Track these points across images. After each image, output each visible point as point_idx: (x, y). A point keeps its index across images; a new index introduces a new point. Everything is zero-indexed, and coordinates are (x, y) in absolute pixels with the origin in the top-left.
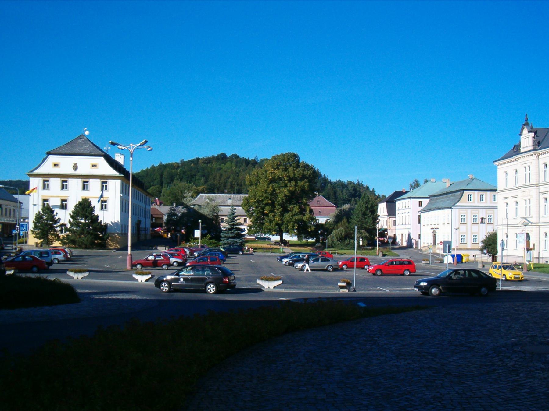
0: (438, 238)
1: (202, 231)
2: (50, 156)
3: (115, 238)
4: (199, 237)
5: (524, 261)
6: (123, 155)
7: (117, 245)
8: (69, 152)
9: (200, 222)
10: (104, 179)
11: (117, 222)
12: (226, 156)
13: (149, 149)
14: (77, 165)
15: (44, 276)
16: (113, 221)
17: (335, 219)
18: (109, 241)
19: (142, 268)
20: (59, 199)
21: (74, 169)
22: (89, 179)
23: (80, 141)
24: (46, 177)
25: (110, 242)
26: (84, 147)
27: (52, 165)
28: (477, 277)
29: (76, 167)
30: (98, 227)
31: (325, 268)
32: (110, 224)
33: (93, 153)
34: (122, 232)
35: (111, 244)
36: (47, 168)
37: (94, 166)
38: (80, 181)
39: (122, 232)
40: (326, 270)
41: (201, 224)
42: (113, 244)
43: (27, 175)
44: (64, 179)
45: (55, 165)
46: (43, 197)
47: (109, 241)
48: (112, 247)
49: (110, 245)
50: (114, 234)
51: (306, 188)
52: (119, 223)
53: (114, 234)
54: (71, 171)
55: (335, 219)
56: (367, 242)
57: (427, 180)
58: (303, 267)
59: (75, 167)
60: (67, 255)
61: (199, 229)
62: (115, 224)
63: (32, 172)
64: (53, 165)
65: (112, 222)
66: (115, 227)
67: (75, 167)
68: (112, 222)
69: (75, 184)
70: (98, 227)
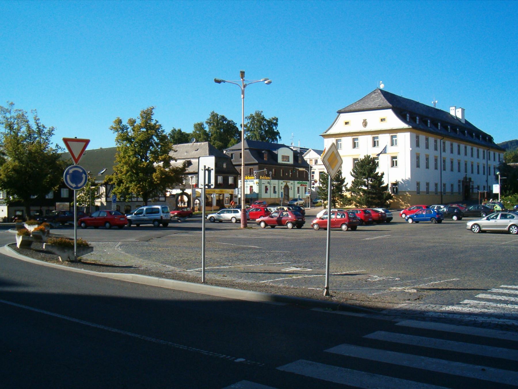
0: (206, 152)
1: (216, 174)
2: (341, 114)
3: (407, 197)
4: (498, 193)
5: (294, 195)
6: (460, 108)
7: (409, 205)
8: (362, 108)
9: (499, 174)
10: (393, 132)
11: (408, 179)
13: (266, 82)
14: (367, 121)
16: (404, 179)
18: (400, 200)
19: (293, 227)
21: (364, 125)
22: (378, 134)
23: (373, 95)
25: (401, 201)
26: (375, 101)
29: (366, 123)
30: (376, 185)
31: (506, 229)
32: (401, 182)
33: (381, 107)
34: (441, 191)
35: (402, 204)
36: (338, 128)
38: (370, 138)
39: (441, 191)
40: (508, 232)
41: (501, 177)
42: (405, 203)
43: (321, 136)
45: (346, 123)
47: (400, 200)
48: (403, 206)
49: (402, 205)
50: (405, 192)
52: (410, 180)
53: (405, 192)
54: (361, 128)
56: (353, 179)
58: (473, 227)
59: (365, 124)
61: (498, 184)
62: (406, 182)
64: (344, 123)
65: (402, 180)
66: (407, 185)
67: (365, 124)
68: (402, 180)
70: (376, 185)
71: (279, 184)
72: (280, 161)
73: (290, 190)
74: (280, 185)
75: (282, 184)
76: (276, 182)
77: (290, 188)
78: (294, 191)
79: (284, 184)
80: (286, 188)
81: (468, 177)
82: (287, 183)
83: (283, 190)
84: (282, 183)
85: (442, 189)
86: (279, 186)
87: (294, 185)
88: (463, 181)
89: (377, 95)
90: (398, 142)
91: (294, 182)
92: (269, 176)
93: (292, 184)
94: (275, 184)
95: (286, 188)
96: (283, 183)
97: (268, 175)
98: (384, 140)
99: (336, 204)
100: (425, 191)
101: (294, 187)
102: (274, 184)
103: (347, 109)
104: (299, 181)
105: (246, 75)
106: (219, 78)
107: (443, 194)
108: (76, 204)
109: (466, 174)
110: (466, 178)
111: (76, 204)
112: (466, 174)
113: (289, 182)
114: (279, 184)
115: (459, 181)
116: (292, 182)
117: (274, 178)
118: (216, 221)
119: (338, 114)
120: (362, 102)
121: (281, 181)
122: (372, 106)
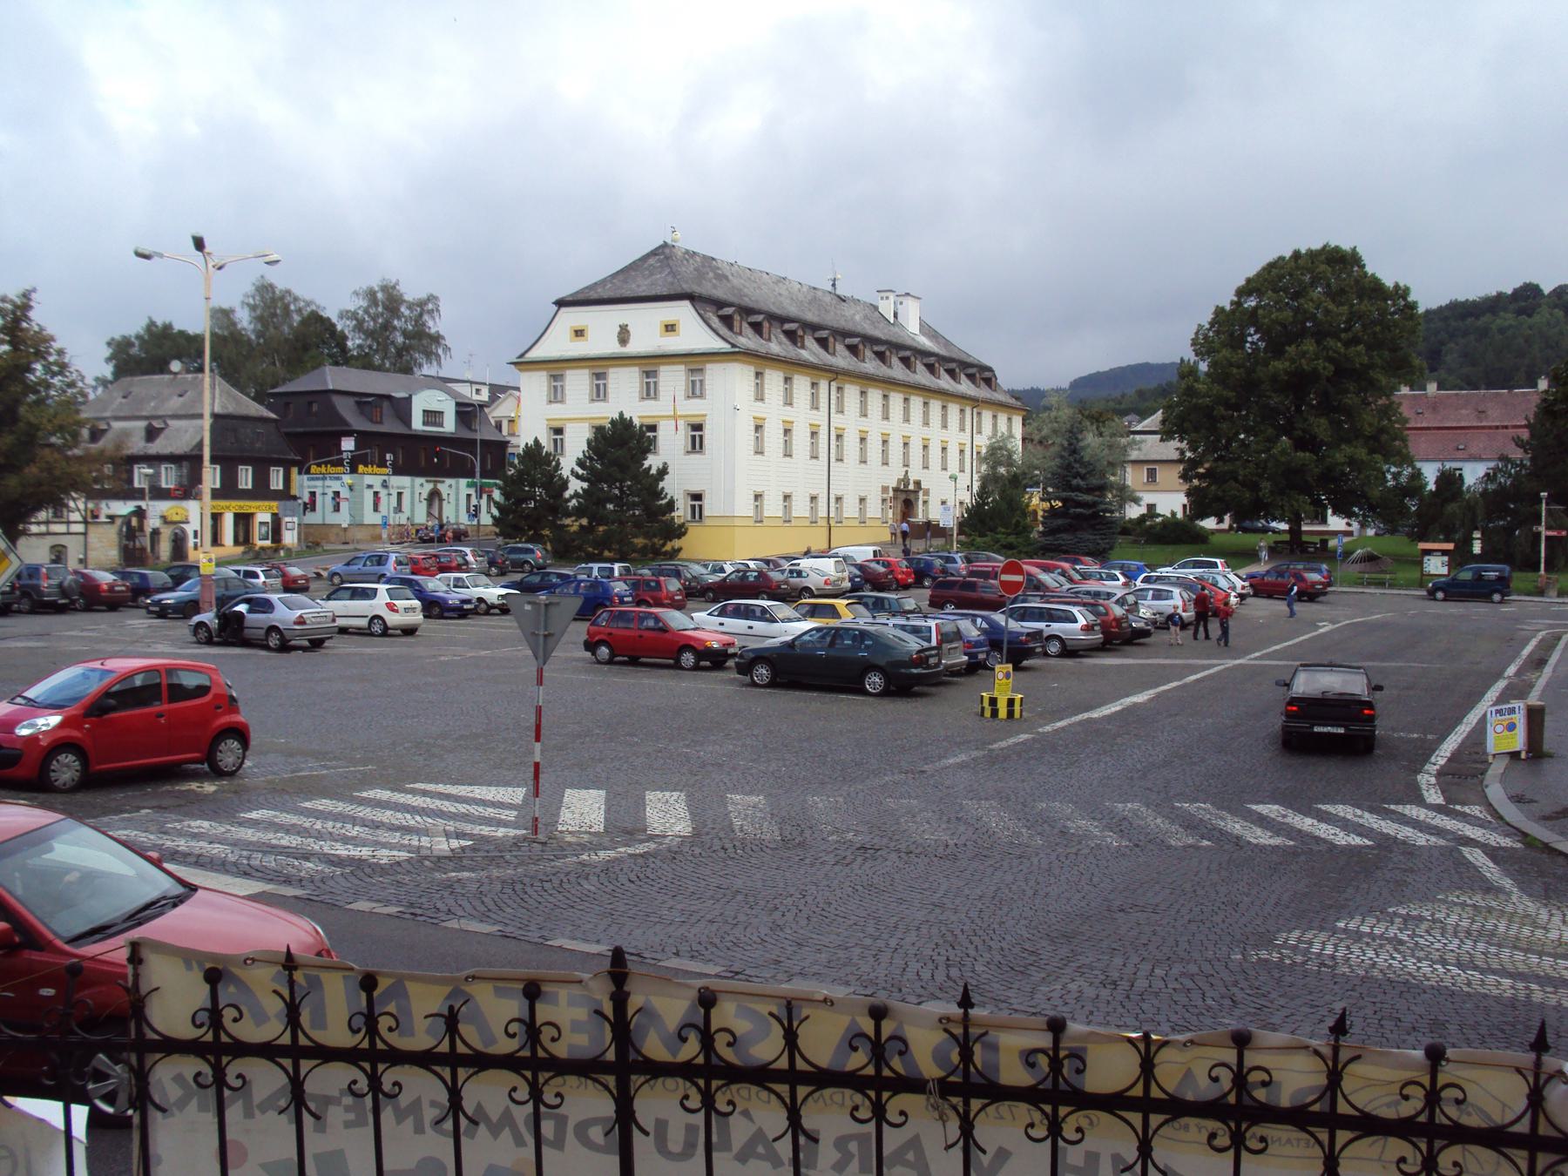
2: (563, 310)
10: (695, 361)
12: (1541, 290)
15: (1501, 685)
17: (47, 509)
20: (587, 425)
24: (556, 368)
27: (569, 334)
28: (8, 929)
37: (670, 328)
43: (512, 366)
44: (599, 366)
46: (551, 423)
51: (1236, 334)
54: (612, 347)
55: (47, 509)
57: (577, 336)
59: (624, 335)
60: (391, 809)
63: (522, 356)
67: (624, 335)
69: (578, 383)
71: (413, 487)
72: (417, 424)
73: (445, 503)
74: (418, 490)
75: (422, 486)
76: (404, 481)
77: (445, 496)
78: (457, 505)
79: (429, 487)
80: (434, 496)
81: (913, 477)
82: (435, 485)
83: (425, 502)
84: (422, 485)
85: (832, 509)
86: (413, 493)
87: (457, 489)
88: (896, 490)
89: (659, 261)
90: (706, 442)
91: (457, 483)
92: (387, 467)
93: (450, 486)
94: (404, 488)
95: (434, 496)
96: (425, 484)
97: (382, 464)
98: (672, 379)
99: (50, 511)
100: (807, 514)
101: (457, 494)
102: (398, 488)
103: (581, 297)
104: (147, 491)
105: (207, 242)
106: (147, 249)
107: (831, 522)
108: (982, 652)
109: (907, 472)
110: (906, 480)
111: (982, 652)
112: (907, 472)
113: (443, 482)
114: (413, 487)
115: (885, 489)
116: (449, 481)
117: (398, 471)
118: (492, 611)
119: (555, 308)
120: (621, 277)
121: (419, 480)
122: (643, 291)
